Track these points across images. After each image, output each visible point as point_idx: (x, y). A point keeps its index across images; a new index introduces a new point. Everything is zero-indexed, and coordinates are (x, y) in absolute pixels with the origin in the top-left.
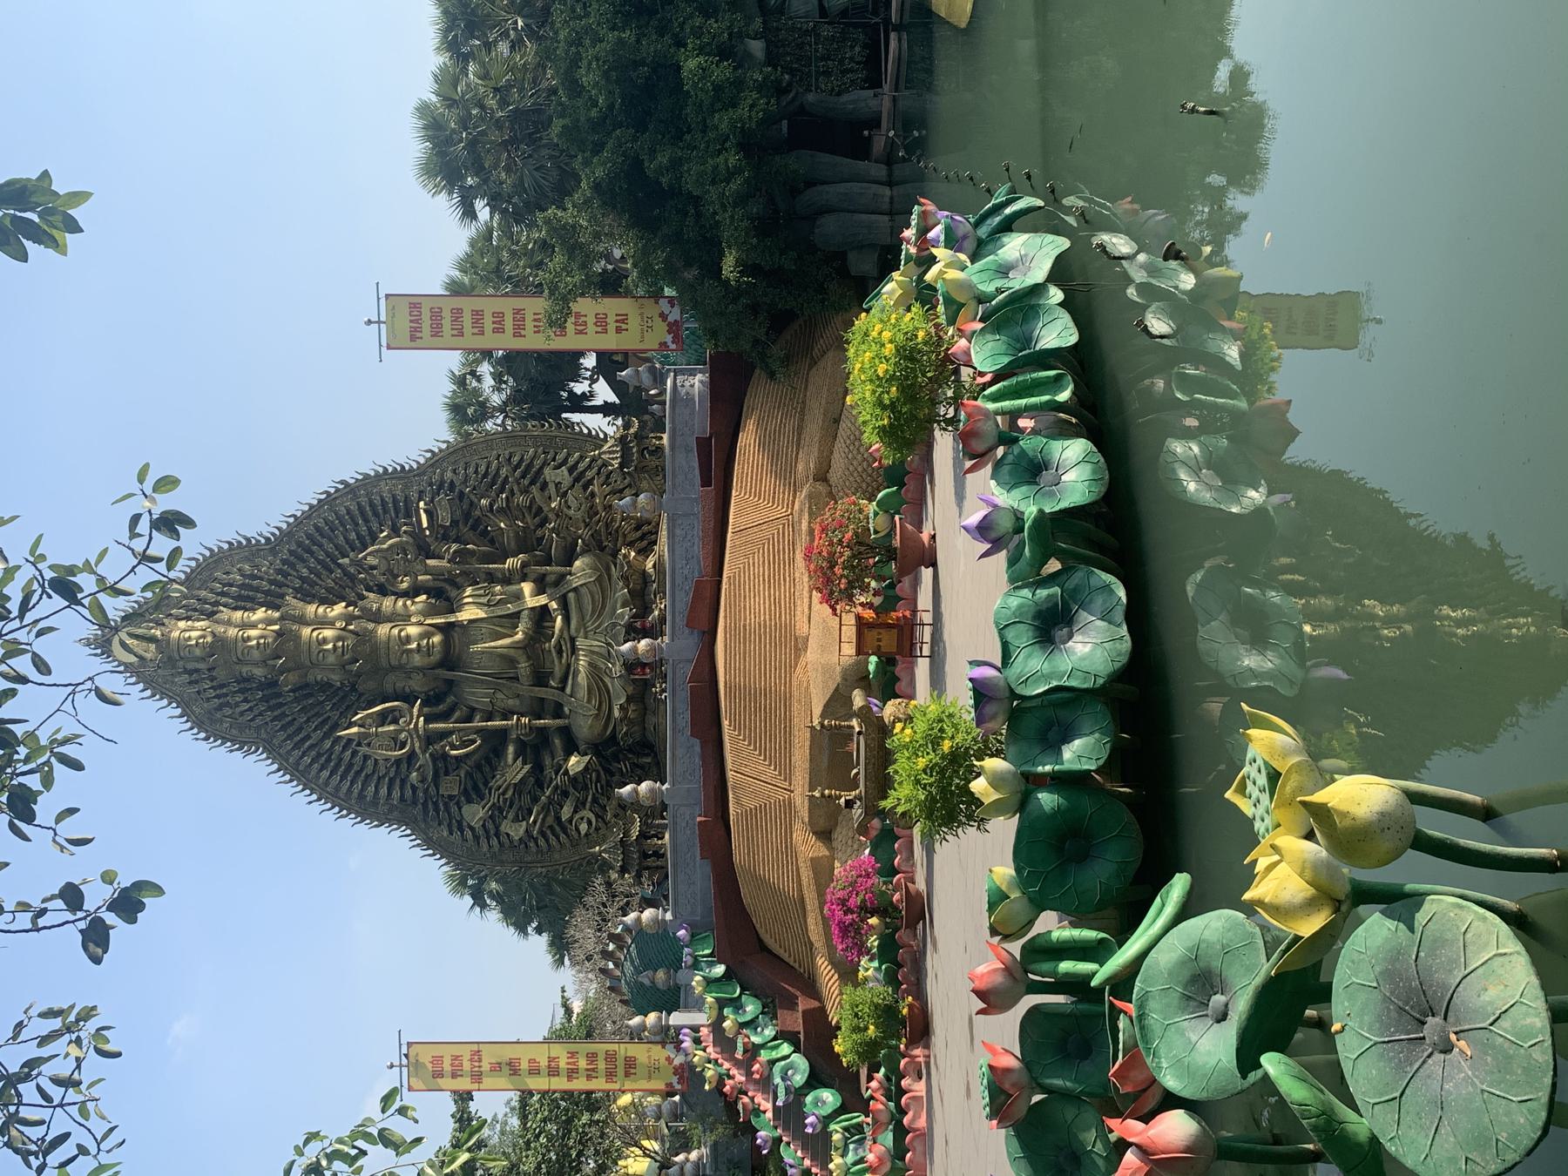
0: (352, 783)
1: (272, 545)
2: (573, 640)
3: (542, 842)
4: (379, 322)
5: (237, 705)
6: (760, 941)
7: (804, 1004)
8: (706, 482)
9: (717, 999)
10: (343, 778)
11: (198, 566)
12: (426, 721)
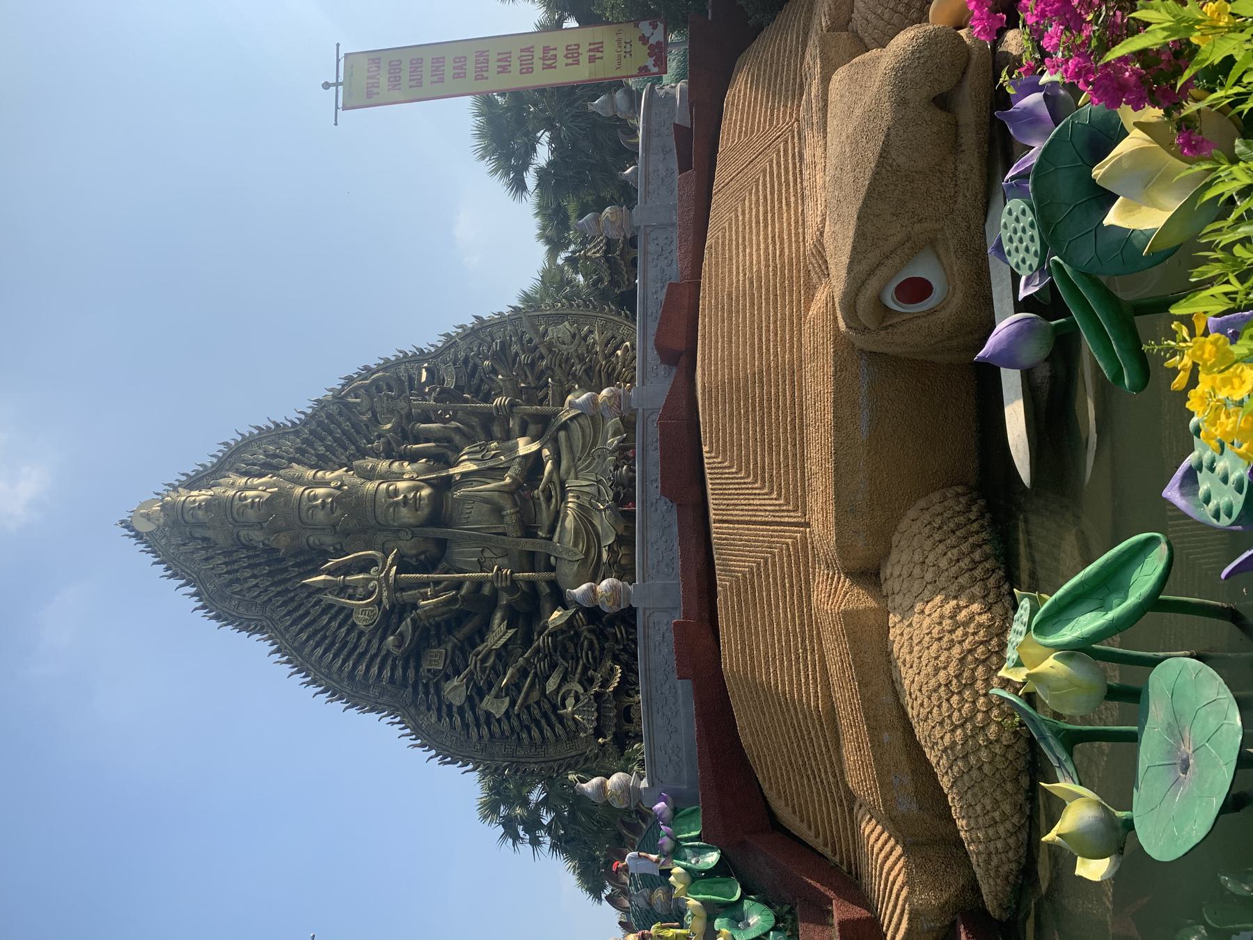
0: (344, 662)
1: (295, 429)
2: (562, 483)
3: (535, 733)
4: (337, 84)
5: (246, 579)
6: (771, 815)
7: (841, 911)
8: (684, 166)
9: (703, 902)
10: (336, 656)
12: (397, 572)
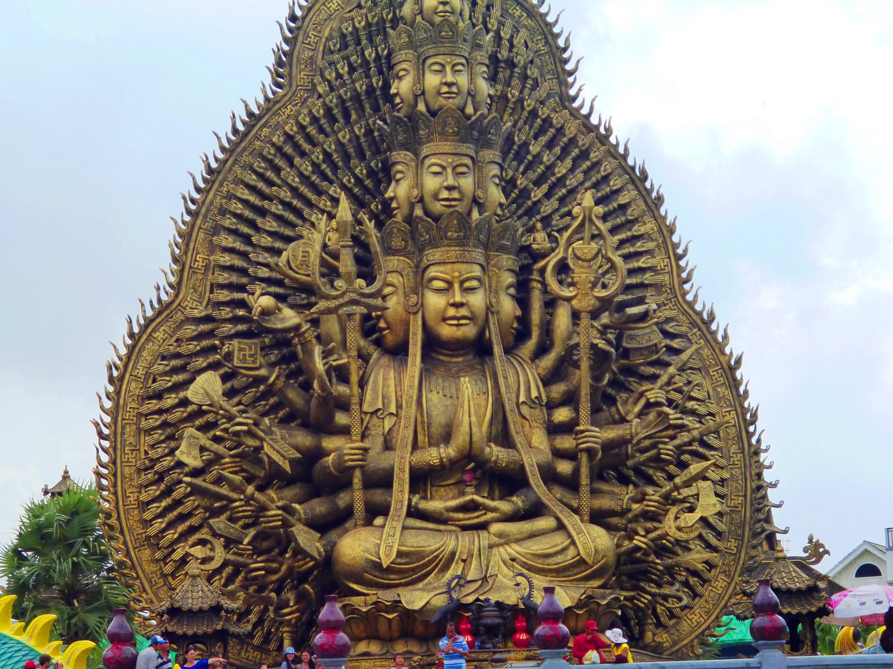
11: (547, 24)
